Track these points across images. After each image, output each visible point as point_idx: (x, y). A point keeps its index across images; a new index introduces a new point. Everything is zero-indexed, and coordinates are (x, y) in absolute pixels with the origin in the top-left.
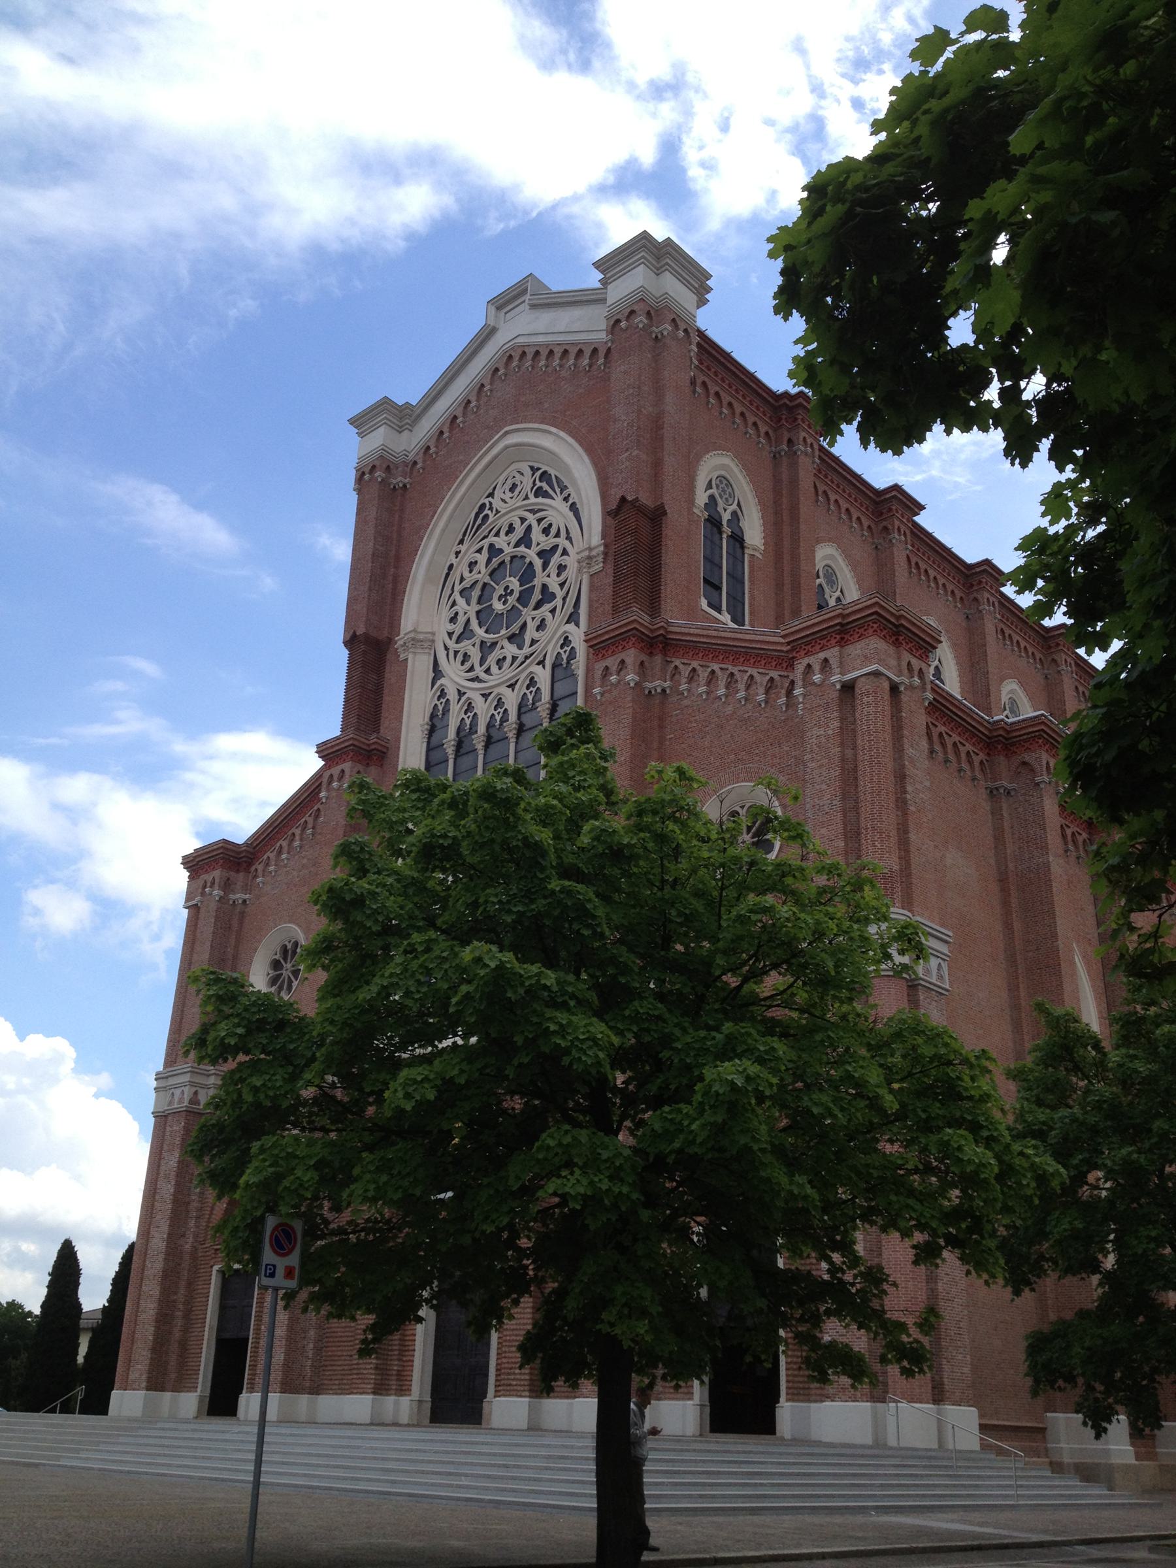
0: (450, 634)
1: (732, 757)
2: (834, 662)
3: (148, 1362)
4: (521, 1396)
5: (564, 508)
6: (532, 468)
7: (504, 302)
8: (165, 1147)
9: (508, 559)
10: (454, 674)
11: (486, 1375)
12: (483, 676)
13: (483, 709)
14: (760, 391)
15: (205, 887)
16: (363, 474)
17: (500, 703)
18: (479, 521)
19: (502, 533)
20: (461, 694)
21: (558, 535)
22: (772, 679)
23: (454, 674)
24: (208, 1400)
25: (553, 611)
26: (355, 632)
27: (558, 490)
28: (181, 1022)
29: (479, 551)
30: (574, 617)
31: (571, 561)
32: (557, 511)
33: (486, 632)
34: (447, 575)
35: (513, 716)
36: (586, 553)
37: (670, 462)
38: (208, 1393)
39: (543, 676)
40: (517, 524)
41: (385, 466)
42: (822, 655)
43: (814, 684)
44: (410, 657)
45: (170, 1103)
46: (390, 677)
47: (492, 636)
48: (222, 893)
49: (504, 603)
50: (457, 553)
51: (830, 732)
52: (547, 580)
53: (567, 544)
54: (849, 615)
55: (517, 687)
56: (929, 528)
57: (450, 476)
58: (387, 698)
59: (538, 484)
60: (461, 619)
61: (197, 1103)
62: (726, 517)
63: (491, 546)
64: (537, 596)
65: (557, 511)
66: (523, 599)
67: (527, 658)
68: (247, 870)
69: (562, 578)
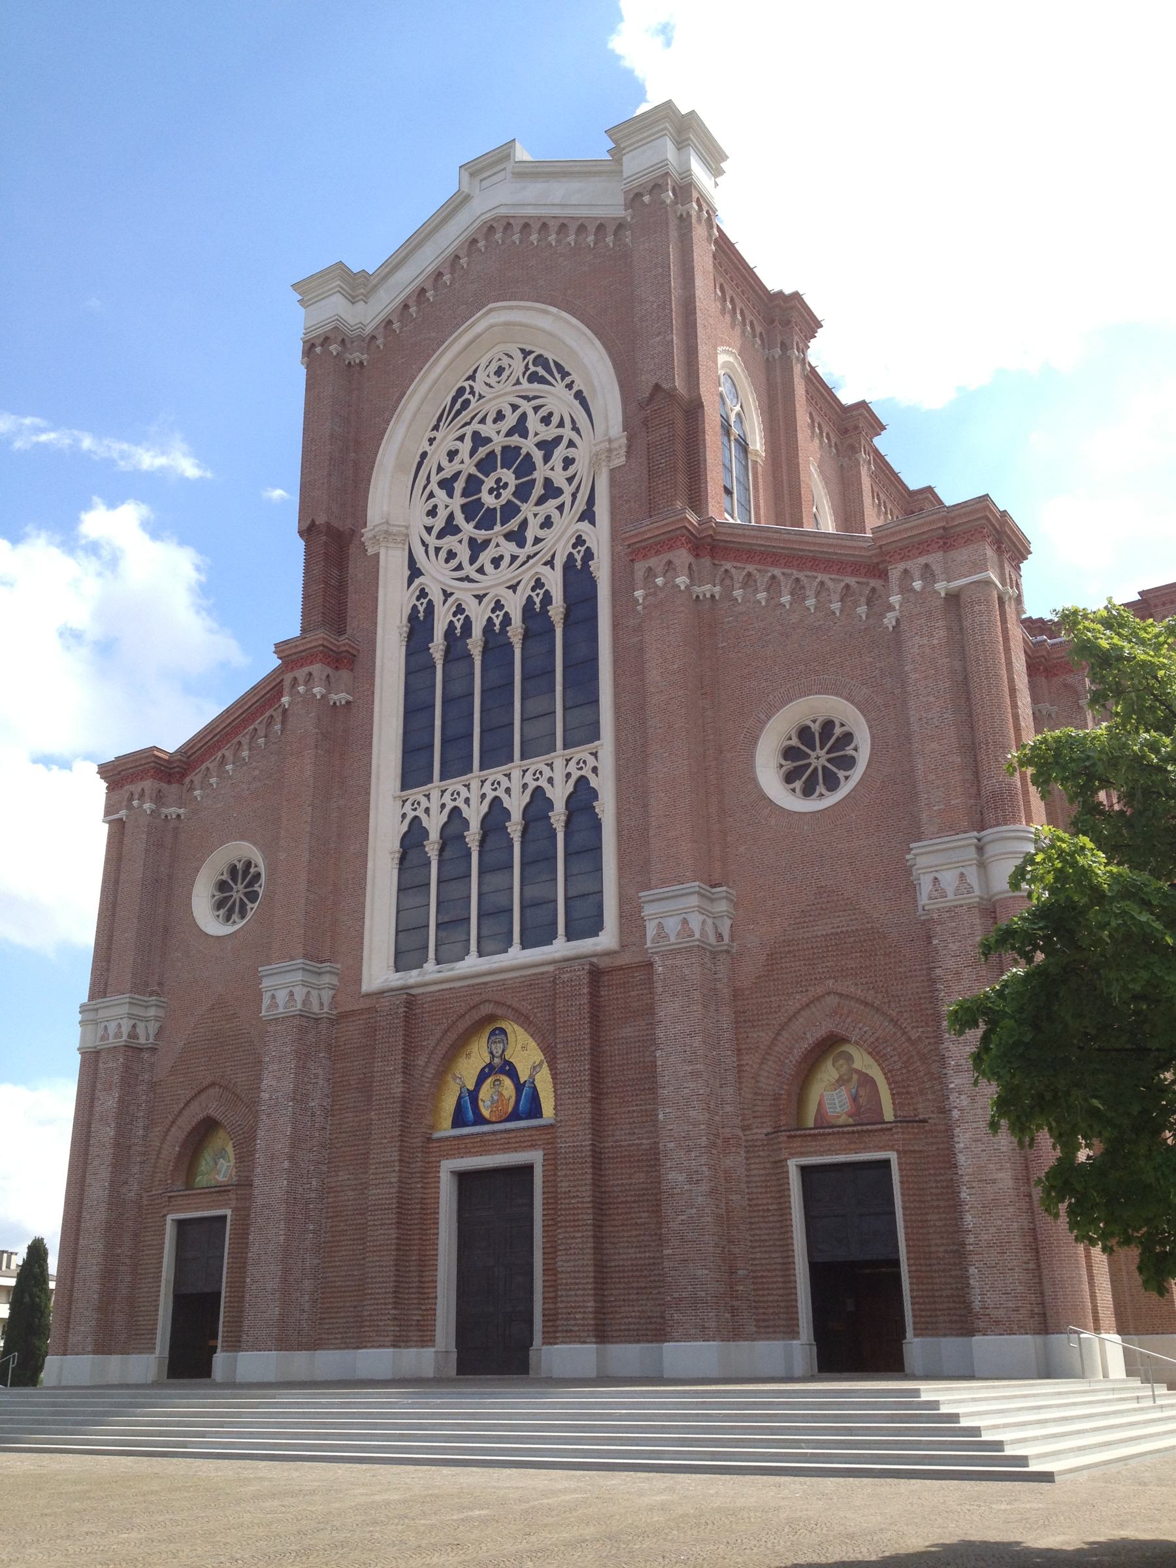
1: (802, 667)
2: (937, 569)
3: (93, 1323)
4: (585, 1342)
5: (569, 396)
6: (522, 350)
7: (477, 170)
8: (99, 1086)
9: (498, 450)
10: (436, 575)
13: (479, 615)
15: (131, 799)
16: (313, 346)
17: (498, 606)
18: (458, 406)
19: (489, 420)
20: (447, 595)
21: (561, 424)
22: (847, 586)
23: (436, 575)
24: (167, 1362)
26: (313, 521)
27: (558, 376)
28: (109, 949)
29: (461, 438)
31: (582, 454)
32: (558, 399)
33: (475, 527)
36: (606, 445)
38: (166, 1354)
40: (507, 411)
41: (340, 339)
43: (913, 590)
44: (382, 552)
45: (103, 1038)
46: (355, 571)
47: (483, 532)
48: (154, 806)
49: (498, 496)
50: (431, 441)
51: (935, 642)
52: (550, 474)
53: (574, 436)
54: (953, 519)
55: (520, 588)
57: (422, 353)
58: (353, 598)
61: (136, 1037)
65: (558, 399)
66: (523, 492)
67: (529, 557)
68: (180, 781)
69: (570, 472)
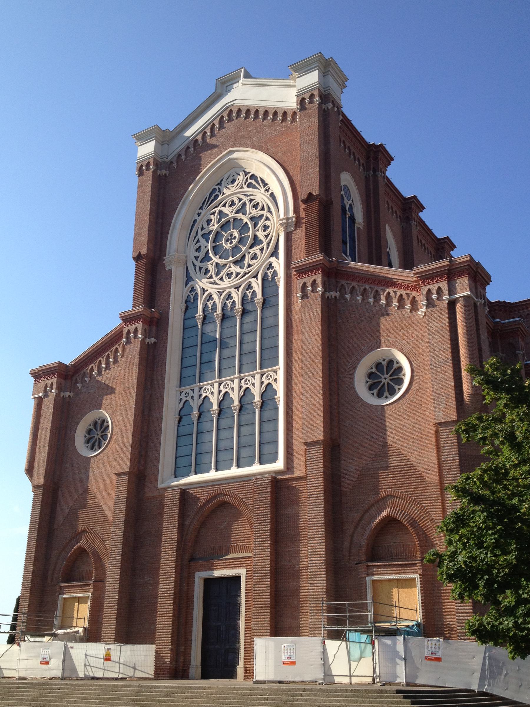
0: (196, 258)
11: (238, 654)
12: (218, 282)
14: (361, 142)
18: (212, 198)
25: (262, 250)
26: (140, 252)
30: (275, 254)
32: (260, 196)
34: (193, 226)
35: (239, 306)
37: (333, 175)
39: (257, 285)
40: (236, 201)
42: (437, 285)
47: (223, 260)
50: (199, 214)
53: (269, 215)
56: (424, 219)
59: (249, 181)
60: (203, 251)
62: (348, 206)
63: (220, 212)
64: (250, 241)
69: (267, 232)
